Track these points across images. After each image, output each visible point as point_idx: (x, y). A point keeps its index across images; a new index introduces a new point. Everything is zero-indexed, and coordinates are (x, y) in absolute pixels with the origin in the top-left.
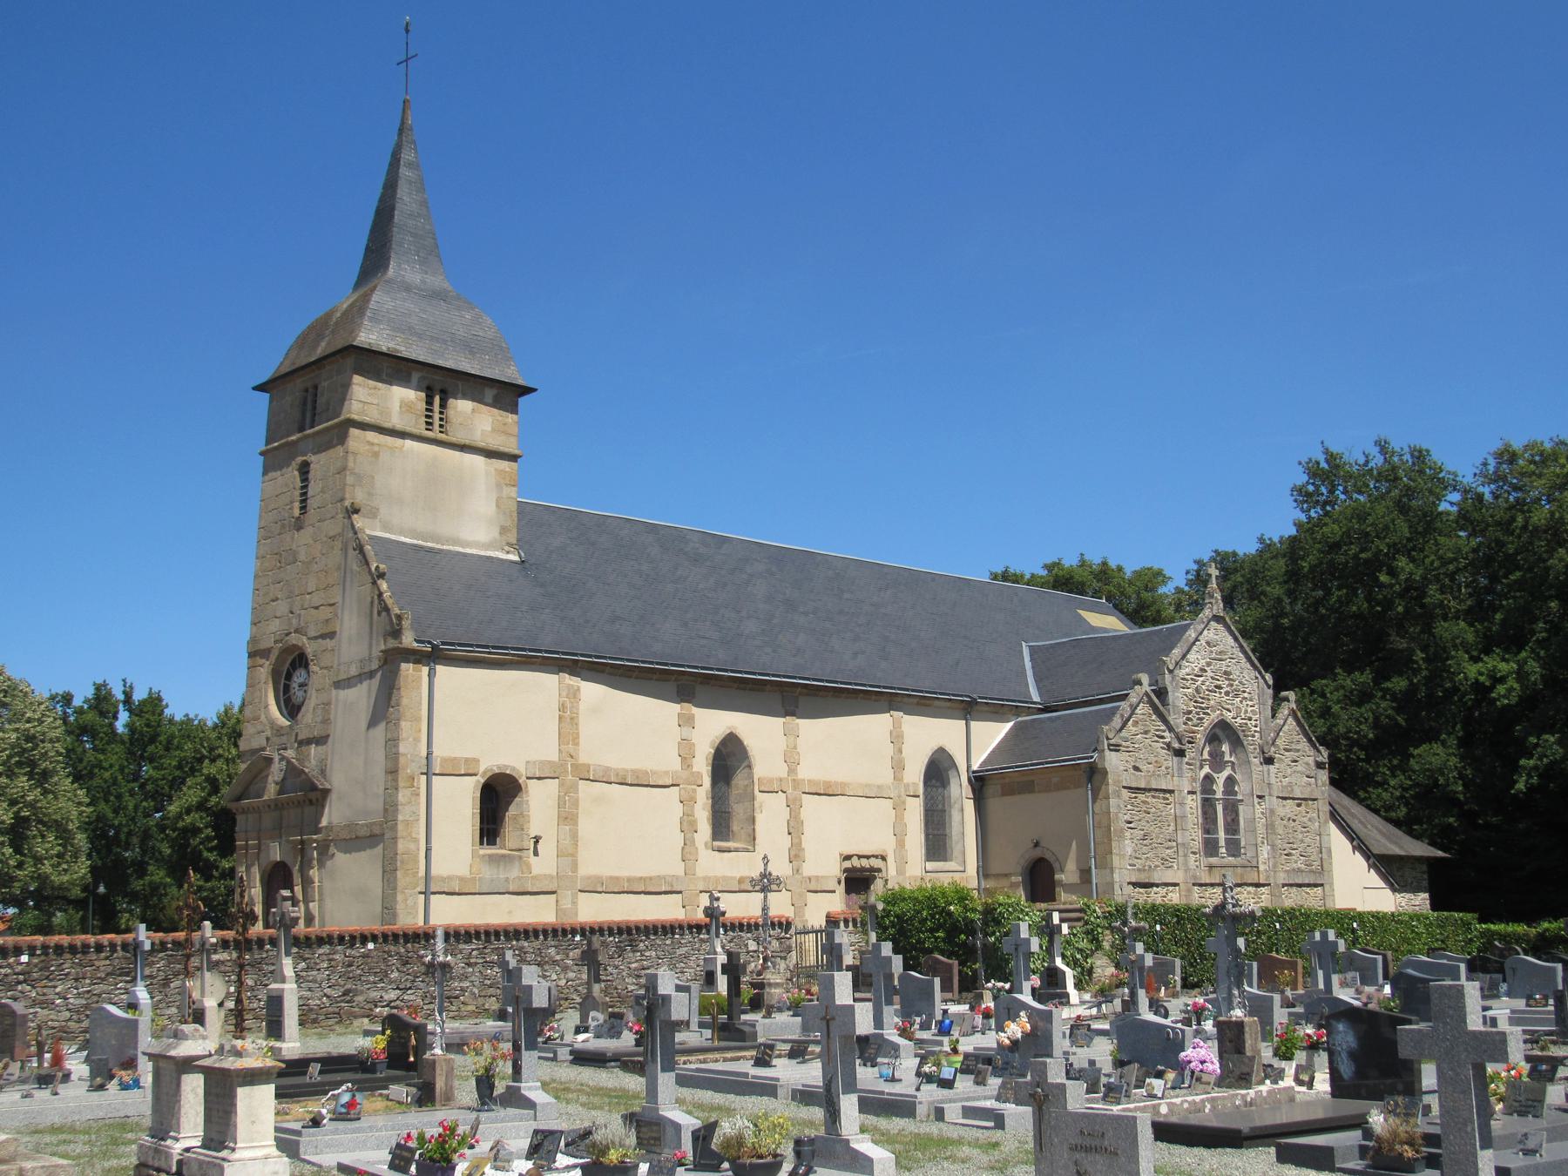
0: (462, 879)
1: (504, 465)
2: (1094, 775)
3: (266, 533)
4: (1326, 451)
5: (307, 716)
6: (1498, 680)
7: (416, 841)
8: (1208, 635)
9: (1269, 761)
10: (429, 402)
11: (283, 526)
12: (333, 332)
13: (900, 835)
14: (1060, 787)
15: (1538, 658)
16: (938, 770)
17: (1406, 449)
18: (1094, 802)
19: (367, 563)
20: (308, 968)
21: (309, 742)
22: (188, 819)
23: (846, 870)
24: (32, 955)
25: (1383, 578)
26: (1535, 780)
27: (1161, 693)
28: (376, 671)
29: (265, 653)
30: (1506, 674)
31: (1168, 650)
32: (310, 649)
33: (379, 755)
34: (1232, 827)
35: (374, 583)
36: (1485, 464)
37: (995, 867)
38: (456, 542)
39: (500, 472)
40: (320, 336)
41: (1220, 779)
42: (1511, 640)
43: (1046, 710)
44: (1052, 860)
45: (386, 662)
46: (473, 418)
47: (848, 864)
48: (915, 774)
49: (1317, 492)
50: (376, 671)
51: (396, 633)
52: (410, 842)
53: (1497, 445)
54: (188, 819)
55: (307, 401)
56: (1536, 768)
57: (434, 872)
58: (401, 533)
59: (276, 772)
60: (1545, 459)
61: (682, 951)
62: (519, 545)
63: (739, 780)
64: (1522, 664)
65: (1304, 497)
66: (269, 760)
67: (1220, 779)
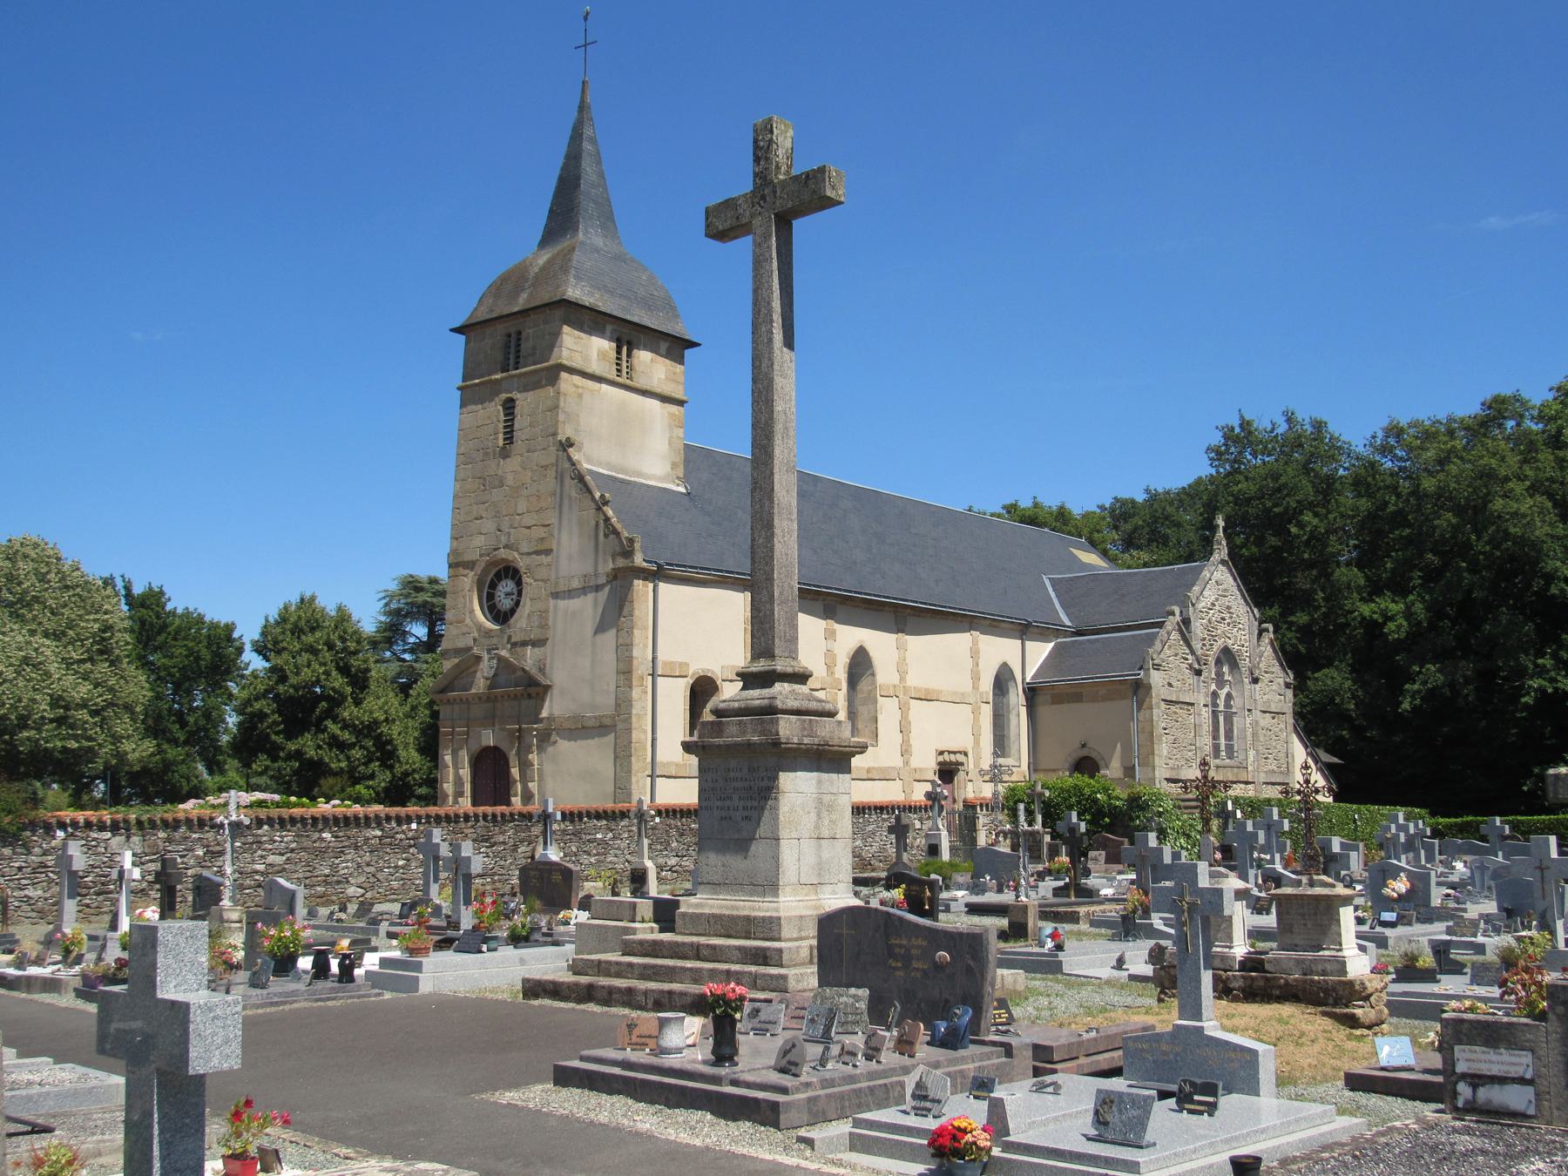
0: (677, 765)
1: (674, 409)
2: (1139, 689)
3: (464, 459)
4: (1242, 417)
5: (522, 622)
6: (1388, 618)
7: (645, 732)
8: (1217, 575)
9: (1255, 681)
10: (619, 352)
11: (486, 454)
12: (533, 285)
13: (976, 735)
14: (1108, 697)
15: (1423, 601)
16: (1002, 681)
17: (1307, 421)
18: (1139, 710)
19: (589, 491)
20: (614, 838)
21: (524, 644)
22: (257, 706)
23: (940, 764)
24: (419, 823)
25: (1294, 530)
26: (1418, 702)
27: (1186, 622)
28: (603, 586)
29: (470, 565)
30: (1395, 613)
31: (1190, 587)
32: (522, 564)
33: (609, 658)
34: (1229, 736)
35: (599, 509)
36: (1374, 437)
37: (1045, 763)
38: (640, 475)
39: (671, 415)
40: (518, 289)
41: (1223, 693)
42: (1400, 588)
43: (1079, 633)
44: (1097, 759)
45: (615, 577)
46: (651, 366)
47: (941, 759)
48: (987, 684)
49: (1227, 452)
50: (603, 586)
51: (628, 554)
52: (640, 735)
53: (1385, 423)
54: (257, 706)
55: (509, 347)
56: (1419, 691)
57: (659, 758)
58: (600, 465)
59: (486, 668)
60: (1428, 435)
61: (870, 828)
62: (685, 479)
63: (863, 686)
64: (1408, 608)
65: (1218, 454)
66: (479, 659)
67: (1223, 693)
